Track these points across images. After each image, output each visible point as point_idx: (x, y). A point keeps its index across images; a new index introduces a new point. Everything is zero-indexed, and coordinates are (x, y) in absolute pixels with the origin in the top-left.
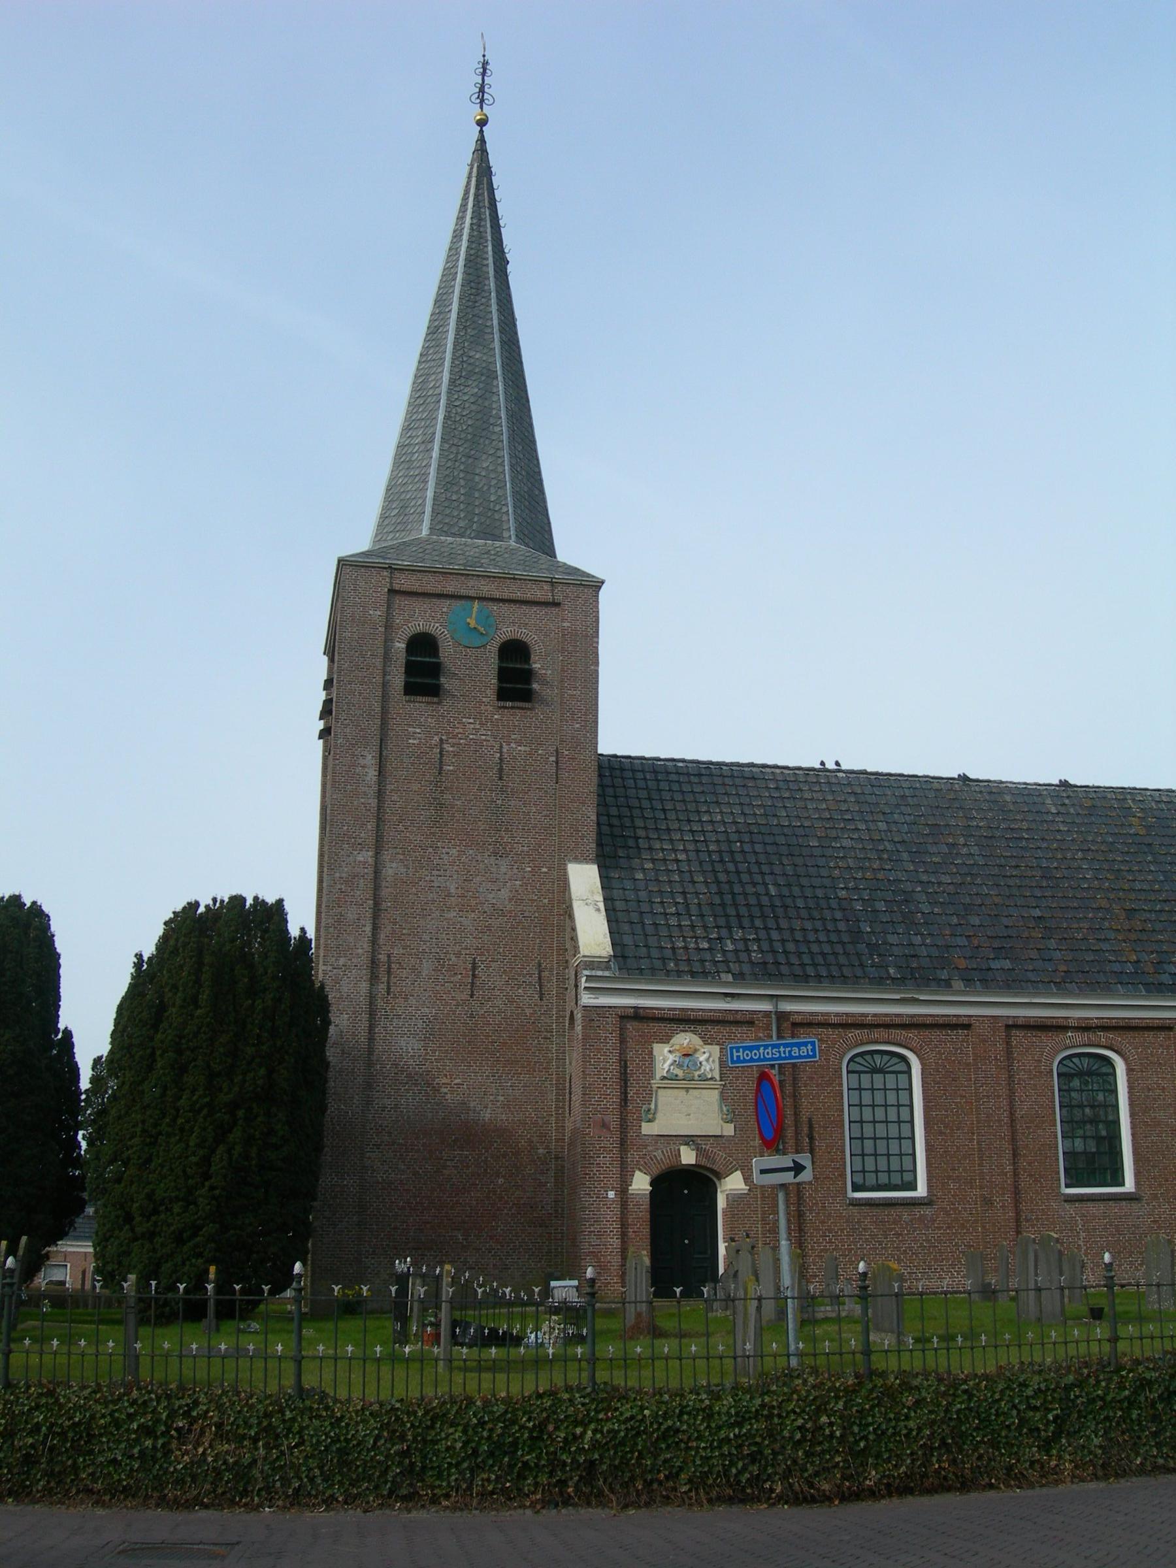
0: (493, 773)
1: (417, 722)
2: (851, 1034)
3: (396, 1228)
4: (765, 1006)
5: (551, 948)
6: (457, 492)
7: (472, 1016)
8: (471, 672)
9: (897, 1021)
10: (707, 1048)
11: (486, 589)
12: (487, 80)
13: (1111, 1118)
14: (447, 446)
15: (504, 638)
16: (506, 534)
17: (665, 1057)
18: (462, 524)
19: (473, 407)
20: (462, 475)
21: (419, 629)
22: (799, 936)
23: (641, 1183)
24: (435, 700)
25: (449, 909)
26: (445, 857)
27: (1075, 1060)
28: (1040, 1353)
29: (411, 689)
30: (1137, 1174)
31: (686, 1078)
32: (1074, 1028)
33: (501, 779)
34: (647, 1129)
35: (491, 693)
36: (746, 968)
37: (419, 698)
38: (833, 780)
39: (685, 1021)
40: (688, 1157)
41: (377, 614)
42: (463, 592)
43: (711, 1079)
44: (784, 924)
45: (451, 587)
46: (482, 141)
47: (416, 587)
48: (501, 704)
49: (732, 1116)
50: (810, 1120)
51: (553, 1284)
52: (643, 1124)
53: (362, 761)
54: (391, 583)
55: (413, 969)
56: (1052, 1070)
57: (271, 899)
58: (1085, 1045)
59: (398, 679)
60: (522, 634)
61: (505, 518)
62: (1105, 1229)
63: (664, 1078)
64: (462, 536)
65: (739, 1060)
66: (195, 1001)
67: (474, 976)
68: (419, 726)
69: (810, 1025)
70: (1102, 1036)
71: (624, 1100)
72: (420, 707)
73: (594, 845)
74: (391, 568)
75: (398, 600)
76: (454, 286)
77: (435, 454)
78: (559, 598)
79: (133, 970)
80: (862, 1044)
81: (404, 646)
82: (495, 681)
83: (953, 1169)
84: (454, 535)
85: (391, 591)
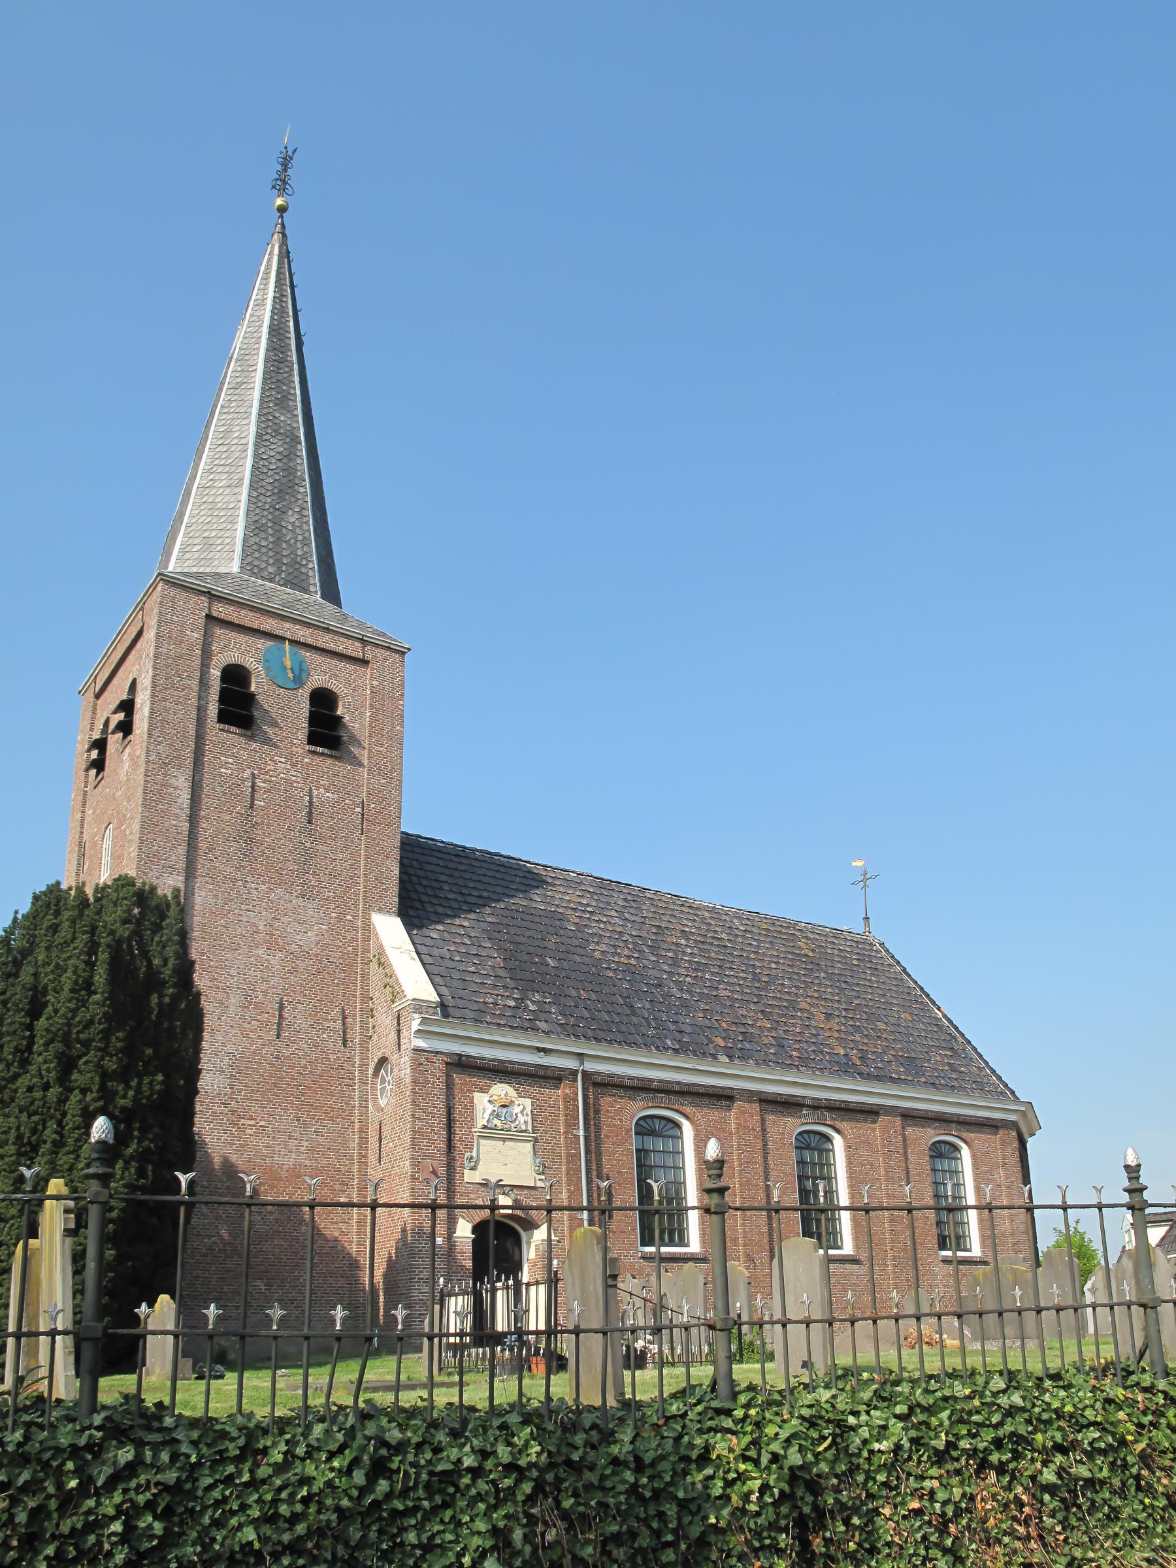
3: (197, 1277)
4: (571, 1064)
5: (355, 996)
7: (278, 1057)
8: (288, 713)
11: (302, 634)
14: (255, 494)
15: (316, 685)
16: (312, 589)
18: (270, 569)
19: (280, 464)
20: (270, 524)
21: (233, 661)
23: (464, 1230)
25: (257, 946)
26: (254, 892)
28: (1019, 1353)
30: (856, 1238)
32: (809, 1106)
33: (310, 822)
34: (469, 1176)
35: (303, 735)
37: (233, 729)
41: (196, 636)
42: (278, 632)
43: (526, 1131)
45: (268, 624)
48: (313, 748)
52: (466, 1171)
53: (173, 781)
54: (210, 609)
55: (221, 1003)
59: (213, 709)
60: (333, 685)
61: (311, 573)
63: (485, 1127)
64: (271, 580)
66: (88, 986)
67: (280, 1016)
68: (232, 757)
71: (450, 1147)
72: (232, 738)
73: (396, 899)
74: (211, 596)
76: (258, 349)
77: (244, 497)
78: (369, 657)
81: (219, 674)
82: (306, 725)
84: (263, 578)
85: (209, 617)
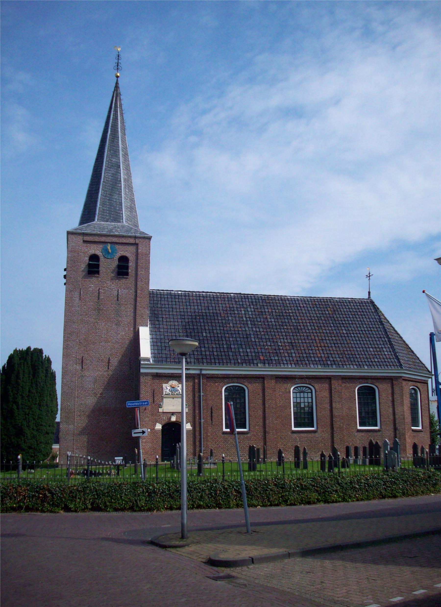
0: (116, 299)
1: (92, 284)
6: (106, 207)
9: (241, 376)
12: (120, 61)
13: (296, 408)
17: (167, 387)
22: (211, 350)
23: (159, 427)
27: (299, 388)
31: (174, 394)
33: (118, 300)
36: (192, 360)
38: (230, 297)
40: (173, 419)
44: (206, 346)
46: (117, 83)
51: (116, 458)
57: (40, 348)
62: (306, 441)
64: (107, 221)
65: (129, 406)
69: (212, 378)
79: (12, 353)
83: (257, 422)
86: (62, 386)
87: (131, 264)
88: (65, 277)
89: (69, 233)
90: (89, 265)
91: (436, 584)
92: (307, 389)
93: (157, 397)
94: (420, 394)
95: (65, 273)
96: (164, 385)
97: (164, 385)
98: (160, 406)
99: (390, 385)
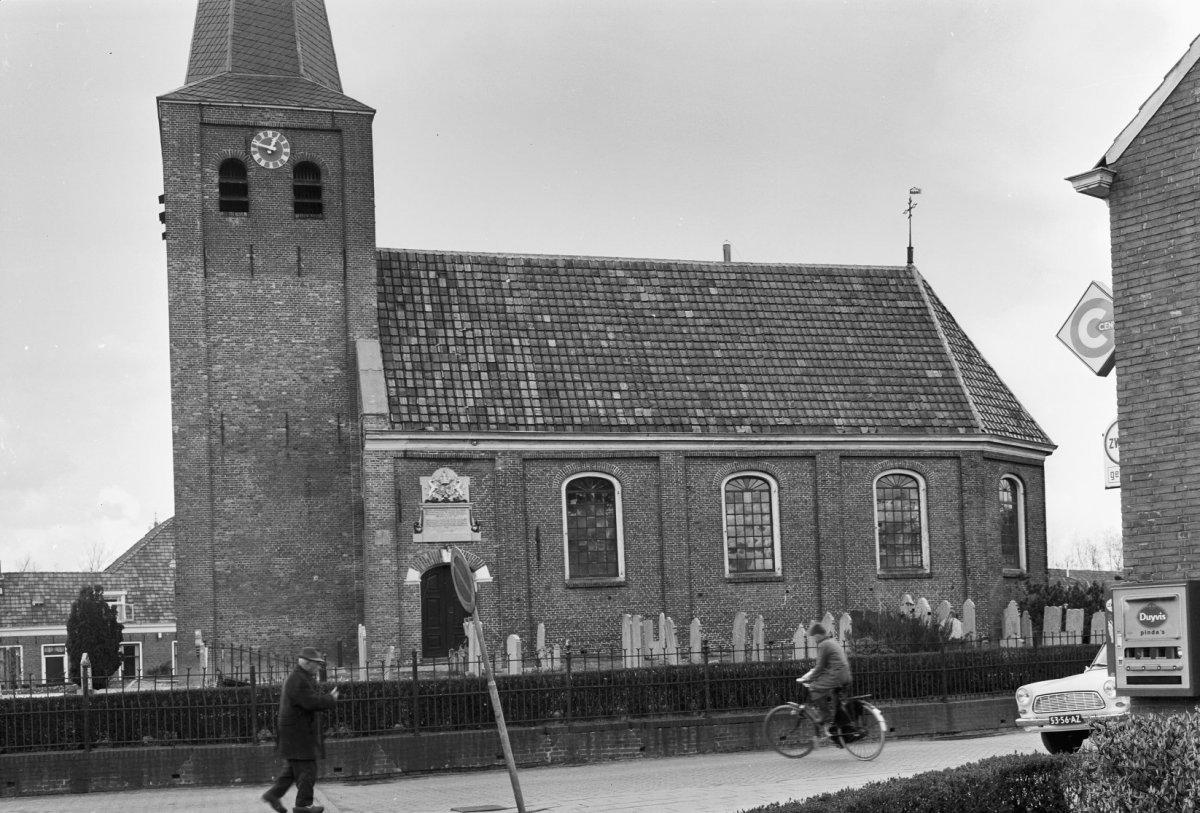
2: (568, 466)
10: (461, 479)
17: (429, 486)
23: (414, 576)
24: (320, 215)
29: (226, 207)
39: (441, 460)
47: (224, 120)
49: (477, 526)
50: (538, 530)
54: (202, 117)
56: (720, 490)
58: (748, 470)
63: (427, 501)
70: (908, 463)
72: (235, 220)
75: (210, 132)
80: (577, 473)
83: (644, 562)
86: (176, 487)
87: (329, 181)
88: (163, 217)
89: (158, 99)
90: (298, 191)
91: (1108, 650)
92: (760, 482)
93: (405, 512)
94: (1025, 494)
95: (162, 208)
96: (424, 481)
97: (424, 481)
98: (417, 528)
99: (507, 774)
